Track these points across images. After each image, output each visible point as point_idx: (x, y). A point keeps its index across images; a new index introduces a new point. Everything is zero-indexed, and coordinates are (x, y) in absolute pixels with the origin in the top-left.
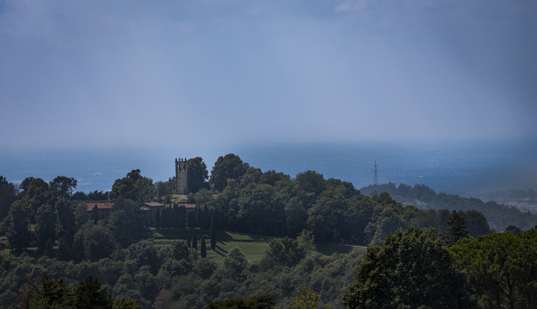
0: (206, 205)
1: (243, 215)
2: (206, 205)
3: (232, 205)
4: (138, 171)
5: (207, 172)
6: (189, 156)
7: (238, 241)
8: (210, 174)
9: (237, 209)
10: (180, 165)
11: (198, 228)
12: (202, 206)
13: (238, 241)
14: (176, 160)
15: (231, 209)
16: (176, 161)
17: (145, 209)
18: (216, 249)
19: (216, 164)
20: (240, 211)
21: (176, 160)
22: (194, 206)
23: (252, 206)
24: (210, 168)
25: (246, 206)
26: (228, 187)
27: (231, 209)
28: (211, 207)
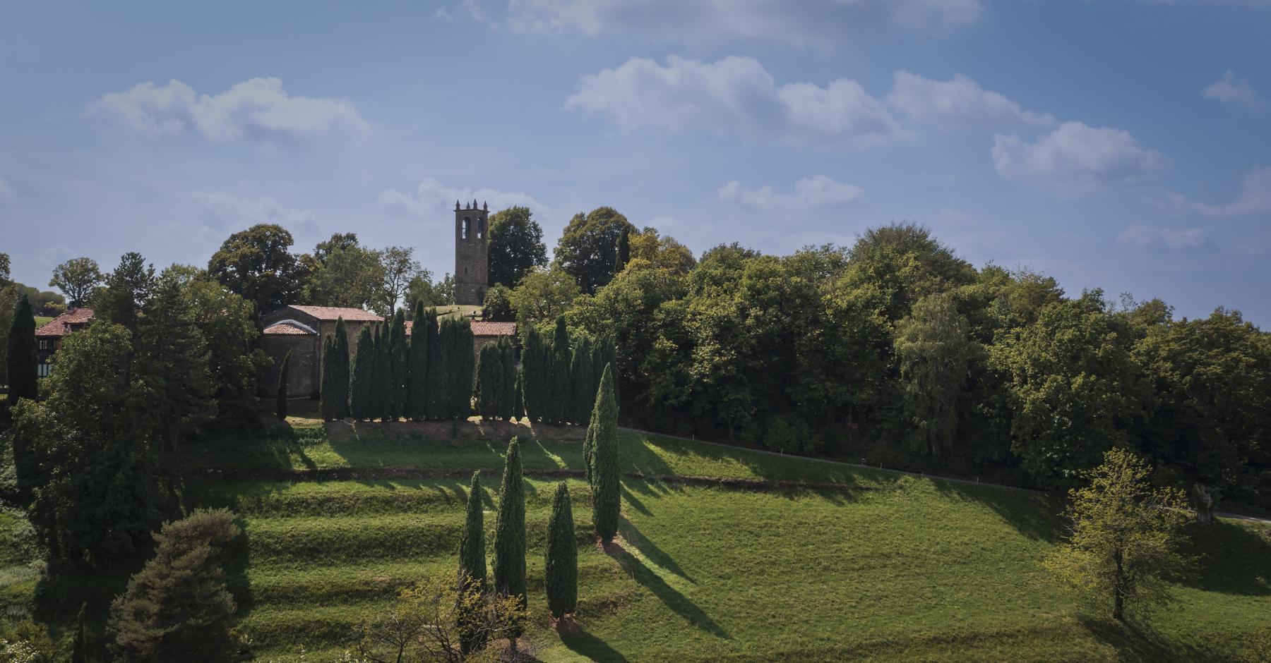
0: (561, 323)
1: (716, 368)
2: (561, 323)
3: (665, 325)
4: (352, 237)
5: (543, 248)
6: (497, 203)
7: (709, 484)
8: (550, 256)
9: (687, 345)
10: (468, 220)
11: (525, 421)
12: (546, 327)
13: (709, 484)
14: (458, 205)
15: (664, 343)
16: (458, 210)
17: (292, 331)
18: (619, 540)
19: (568, 230)
20: (704, 351)
21: (458, 205)
22: (507, 329)
23: (749, 329)
24: (551, 240)
25: (725, 331)
26: (633, 261)
27: (664, 343)
28: (580, 332)
